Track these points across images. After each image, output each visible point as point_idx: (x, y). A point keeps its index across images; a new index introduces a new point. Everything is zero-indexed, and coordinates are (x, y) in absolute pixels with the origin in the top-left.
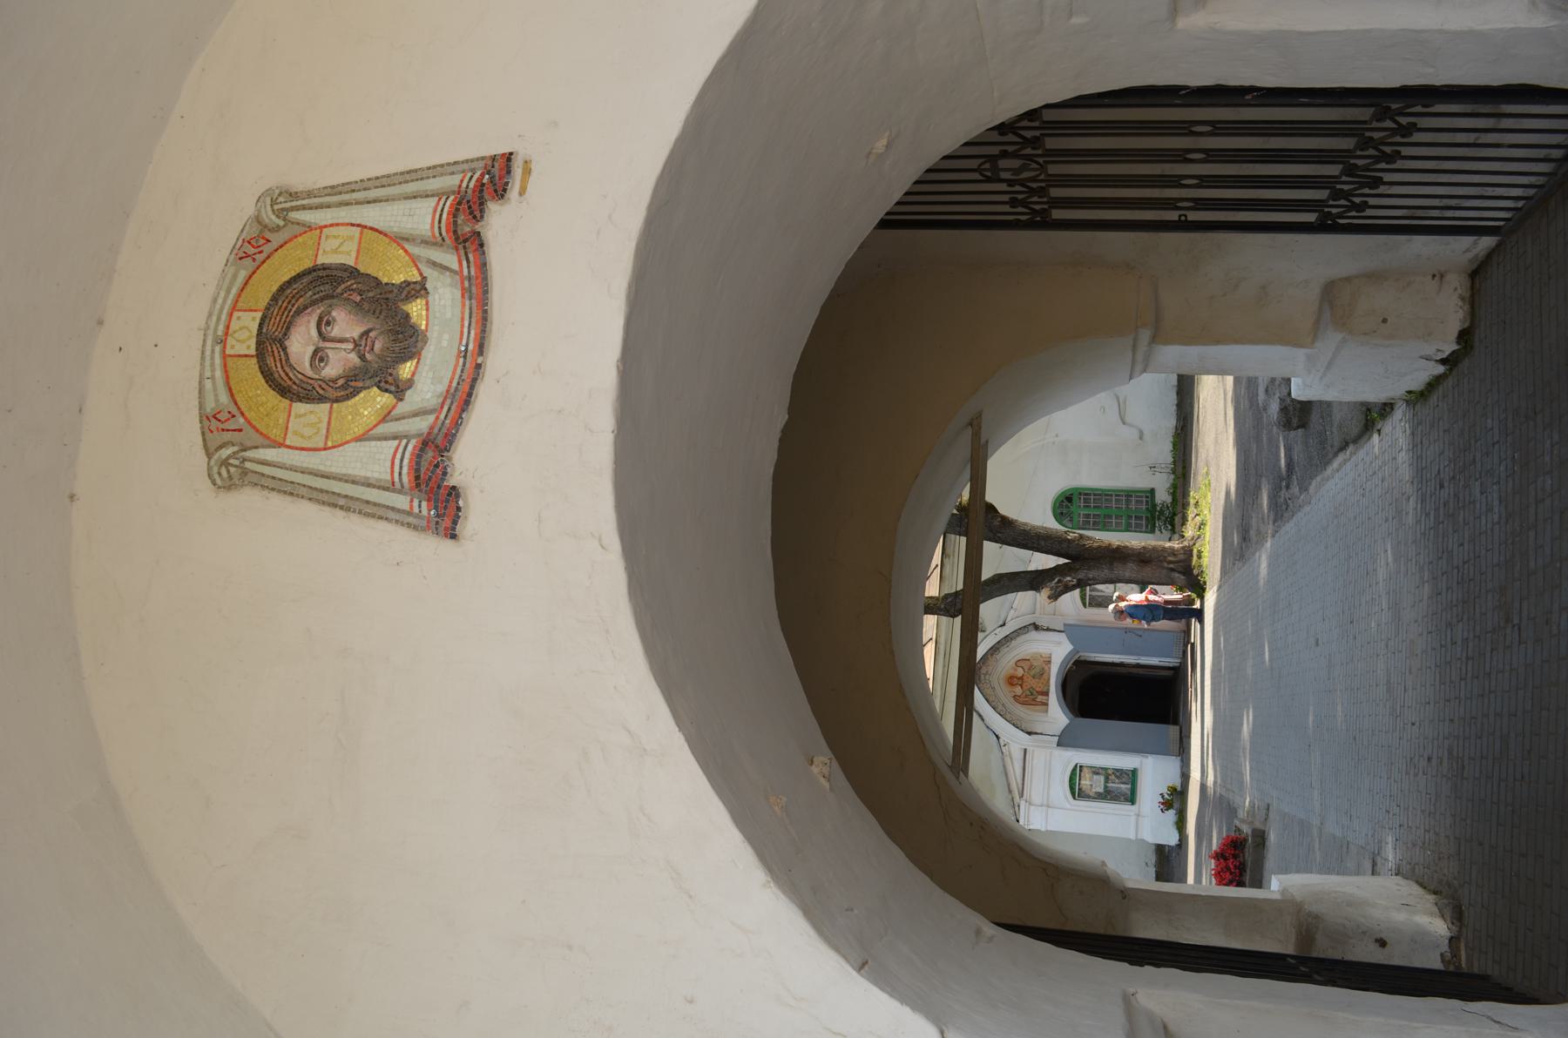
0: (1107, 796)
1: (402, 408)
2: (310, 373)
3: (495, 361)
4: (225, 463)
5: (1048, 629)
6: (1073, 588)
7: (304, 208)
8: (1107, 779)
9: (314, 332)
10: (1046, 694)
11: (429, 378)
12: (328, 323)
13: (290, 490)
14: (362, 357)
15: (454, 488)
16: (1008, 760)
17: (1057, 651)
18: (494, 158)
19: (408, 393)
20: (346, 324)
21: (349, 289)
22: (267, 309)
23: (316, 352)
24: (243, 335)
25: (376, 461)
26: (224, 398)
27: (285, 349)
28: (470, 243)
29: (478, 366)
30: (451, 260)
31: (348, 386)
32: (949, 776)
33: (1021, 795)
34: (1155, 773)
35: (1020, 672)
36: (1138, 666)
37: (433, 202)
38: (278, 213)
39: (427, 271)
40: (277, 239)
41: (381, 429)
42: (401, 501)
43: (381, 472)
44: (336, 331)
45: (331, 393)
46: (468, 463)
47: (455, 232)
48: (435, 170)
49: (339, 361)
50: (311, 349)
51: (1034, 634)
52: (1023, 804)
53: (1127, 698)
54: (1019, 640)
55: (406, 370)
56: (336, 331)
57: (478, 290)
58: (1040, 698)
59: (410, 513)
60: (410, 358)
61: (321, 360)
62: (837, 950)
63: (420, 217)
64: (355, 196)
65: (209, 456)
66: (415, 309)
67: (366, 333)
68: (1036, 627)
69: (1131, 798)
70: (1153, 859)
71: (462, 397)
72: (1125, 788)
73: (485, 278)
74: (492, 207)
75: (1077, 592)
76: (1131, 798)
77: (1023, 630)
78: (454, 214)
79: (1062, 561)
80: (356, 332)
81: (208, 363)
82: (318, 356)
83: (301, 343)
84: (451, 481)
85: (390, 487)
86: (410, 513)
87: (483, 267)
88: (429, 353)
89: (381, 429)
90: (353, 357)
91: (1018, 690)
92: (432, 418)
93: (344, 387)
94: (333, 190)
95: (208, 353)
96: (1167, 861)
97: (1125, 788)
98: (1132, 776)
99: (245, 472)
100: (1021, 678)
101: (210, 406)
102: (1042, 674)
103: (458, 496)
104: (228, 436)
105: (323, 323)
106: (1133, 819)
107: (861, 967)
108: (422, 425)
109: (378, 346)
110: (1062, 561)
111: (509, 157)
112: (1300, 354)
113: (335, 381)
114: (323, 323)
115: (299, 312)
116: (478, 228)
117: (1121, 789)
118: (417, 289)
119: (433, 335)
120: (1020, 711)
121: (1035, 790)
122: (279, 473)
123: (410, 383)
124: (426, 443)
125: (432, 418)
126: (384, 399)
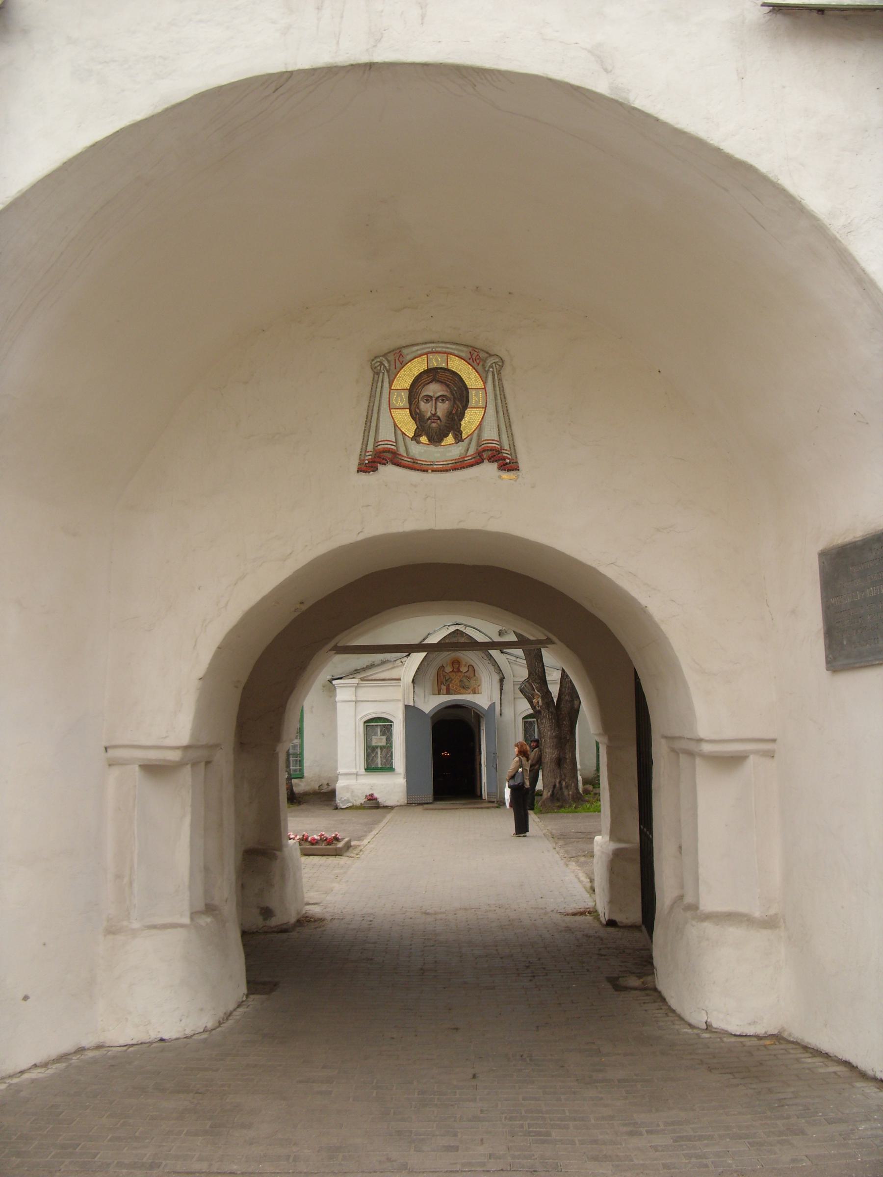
0: (370, 751)
1: (408, 441)
2: (422, 395)
3: (429, 477)
4: (381, 364)
5: (501, 689)
6: (533, 707)
7: (494, 378)
8: (382, 748)
9: (439, 394)
11: (422, 450)
12: (443, 400)
13: (372, 396)
14: (429, 419)
15: (377, 469)
16: (390, 665)
17: (483, 698)
18: (517, 462)
19: (414, 442)
20: (442, 408)
21: (458, 406)
22: (449, 370)
23: (431, 397)
24: (437, 360)
25: (386, 434)
26: (409, 358)
27: (431, 382)
28: (478, 460)
29: (427, 471)
30: (471, 451)
31: (416, 415)
32: (331, 645)
33: (362, 679)
34: (392, 786)
35: (464, 669)
36: (480, 765)
37: (497, 438)
38: (491, 366)
39: (466, 441)
40: (480, 368)
41: (399, 432)
42: (370, 447)
43: (381, 438)
44: (439, 404)
45: (413, 407)
46: (388, 471)
47: (484, 451)
48: (511, 436)
49: (426, 408)
50: (431, 394)
51: (496, 678)
52: (356, 681)
53: (451, 762)
54: (491, 668)
55: (424, 439)
56: (439, 404)
57: (459, 465)
58: (444, 688)
59: (366, 451)
60: (429, 441)
61: (427, 400)
62: (224, 639)
63: (490, 434)
64: (499, 401)
65: (385, 355)
66: (450, 439)
67: (439, 418)
68: (502, 681)
69: (370, 768)
70: (325, 789)
71: (415, 466)
72: (379, 762)
73: (464, 468)
74: (495, 465)
75: (531, 711)
76: (370, 768)
77: (499, 671)
78: (492, 449)
79: (555, 700)
80: (439, 414)
81: (424, 346)
82: (428, 399)
83: (434, 389)
84: (380, 467)
85: (376, 441)
86: (366, 451)
87: (471, 465)
88: (432, 448)
89: (399, 432)
90: (429, 414)
91: (448, 669)
92: (405, 455)
93: (416, 413)
94: (502, 390)
95: (428, 345)
96: (325, 797)
97: (379, 762)
98: (388, 767)
99: (378, 374)
100: (459, 671)
101: (405, 351)
102: (464, 688)
103: (374, 471)
104: (393, 363)
105: (443, 398)
106: (354, 771)
107: (219, 648)
108: (402, 451)
109: (434, 425)
110: (555, 700)
111: (517, 469)
112: (607, 838)
113: (418, 408)
114: (443, 398)
115: (448, 386)
116: (486, 461)
117: (376, 760)
118: (458, 438)
119: (440, 449)
120: (432, 672)
121: (368, 692)
122: (379, 390)
123: (419, 442)
124: (395, 454)
125: (405, 455)
126: (411, 435)
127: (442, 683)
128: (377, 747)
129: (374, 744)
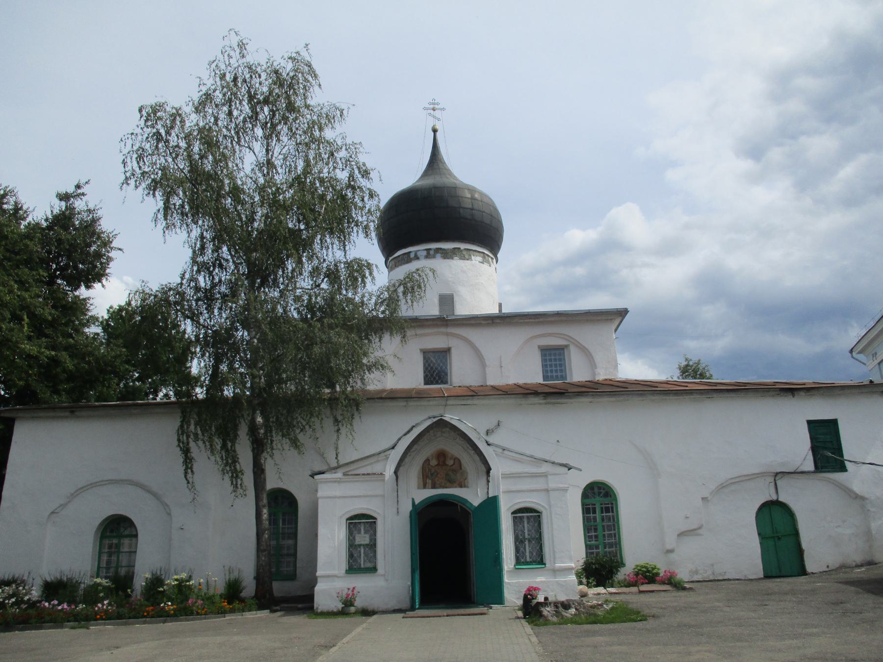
0: (352, 546)
10: (434, 487)
35: (450, 462)
58: (429, 481)
100: (444, 464)
127: (427, 477)
128: (360, 546)
129: (357, 543)
